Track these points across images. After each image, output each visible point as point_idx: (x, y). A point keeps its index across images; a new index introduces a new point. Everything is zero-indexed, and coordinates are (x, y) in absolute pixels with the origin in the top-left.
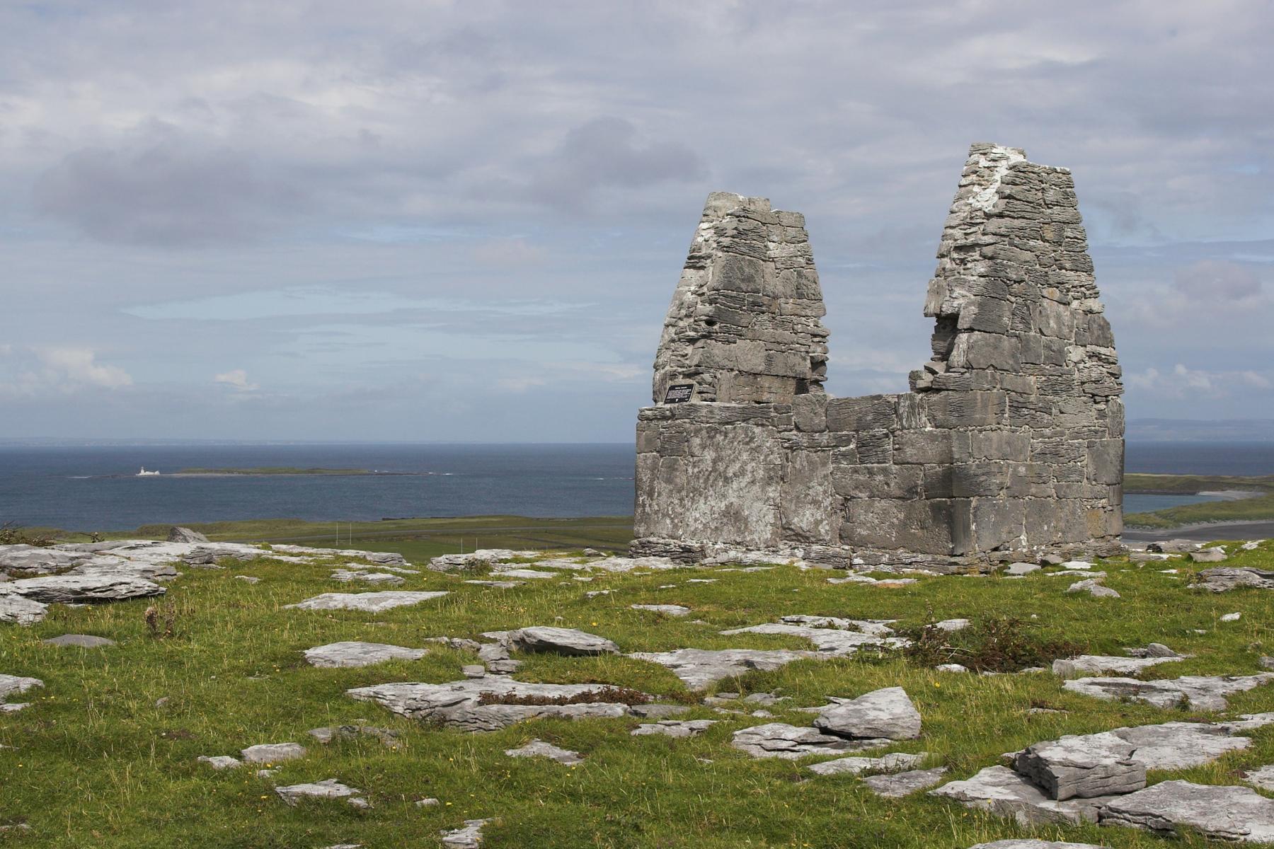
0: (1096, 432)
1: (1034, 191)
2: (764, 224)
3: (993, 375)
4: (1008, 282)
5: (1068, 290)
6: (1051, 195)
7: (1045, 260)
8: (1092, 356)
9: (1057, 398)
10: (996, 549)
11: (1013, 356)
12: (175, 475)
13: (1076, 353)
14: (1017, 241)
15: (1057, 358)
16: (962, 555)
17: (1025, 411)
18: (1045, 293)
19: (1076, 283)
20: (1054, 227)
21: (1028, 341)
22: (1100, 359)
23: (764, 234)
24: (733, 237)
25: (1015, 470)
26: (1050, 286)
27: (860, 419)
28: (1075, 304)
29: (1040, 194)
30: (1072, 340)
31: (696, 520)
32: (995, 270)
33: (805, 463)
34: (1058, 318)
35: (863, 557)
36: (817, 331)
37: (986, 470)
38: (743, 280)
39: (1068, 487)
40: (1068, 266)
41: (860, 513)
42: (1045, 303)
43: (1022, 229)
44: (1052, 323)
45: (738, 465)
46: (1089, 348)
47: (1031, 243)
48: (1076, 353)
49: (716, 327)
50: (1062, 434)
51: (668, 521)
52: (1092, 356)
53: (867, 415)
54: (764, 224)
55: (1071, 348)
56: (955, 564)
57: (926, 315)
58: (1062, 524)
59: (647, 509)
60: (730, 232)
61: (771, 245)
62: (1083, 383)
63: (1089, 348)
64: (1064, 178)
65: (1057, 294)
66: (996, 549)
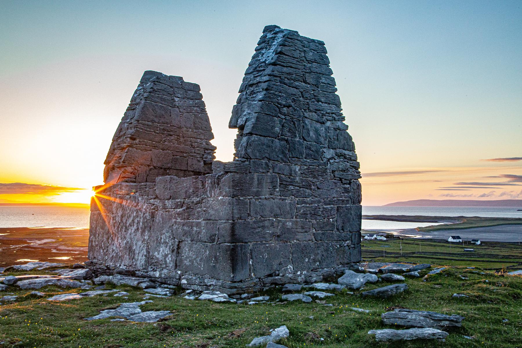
0: (343, 201)
1: (298, 52)
2: (171, 87)
3: (267, 164)
4: (280, 106)
5: (323, 115)
6: (310, 55)
7: (307, 95)
8: (339, 156)
9: (315, 180)
10: (270, 275)
11: (283, 152)
12: (443, 224)
13: (329, 153)
14: (286, 81)
15: (316, 155)
16: (241, 281)
17: (292, 187)
18: (306, 115)
19: (328, 111)
20: (313, 75)
21: (294, 144)
22: (345, 158)
23: (171, 93)
24: (150, 92)
25: (284, 224)
26: (311, 111)
27: (186, 192)
28: (328, 124)
29: (303, 54)
30: (326, 146)
31: (113, 251)
32: (270, 97)
33: (161, 219)
34: (316, 131)
35: (187, 280)
36: (207, 147)
37: (261, 224)
38: (156, 117)
39: (323, 234)
40: (323, 100)
41: (186, 251)
42: (307, 121)
43: (289, 74)
44: (312, 134)
45: (131, 219)
46: (338, 151)
47: (297, 83)
48: (329, 153)
49: (137, 141)
50: (319, 202)
51: (102, 251)
52: (339, 156)
53: (190, 189)
54: (171, 87)
55: (325, 150)
56: (236, 287)
57: (231, 126)
58: (319, 257)
59: (94, 243)
60: (148, 90)
61: (177, 99)
62: (333, 172)
63: (338, 151)
64: (320, 47)
65: (315, 116)
66: (270, 275)
